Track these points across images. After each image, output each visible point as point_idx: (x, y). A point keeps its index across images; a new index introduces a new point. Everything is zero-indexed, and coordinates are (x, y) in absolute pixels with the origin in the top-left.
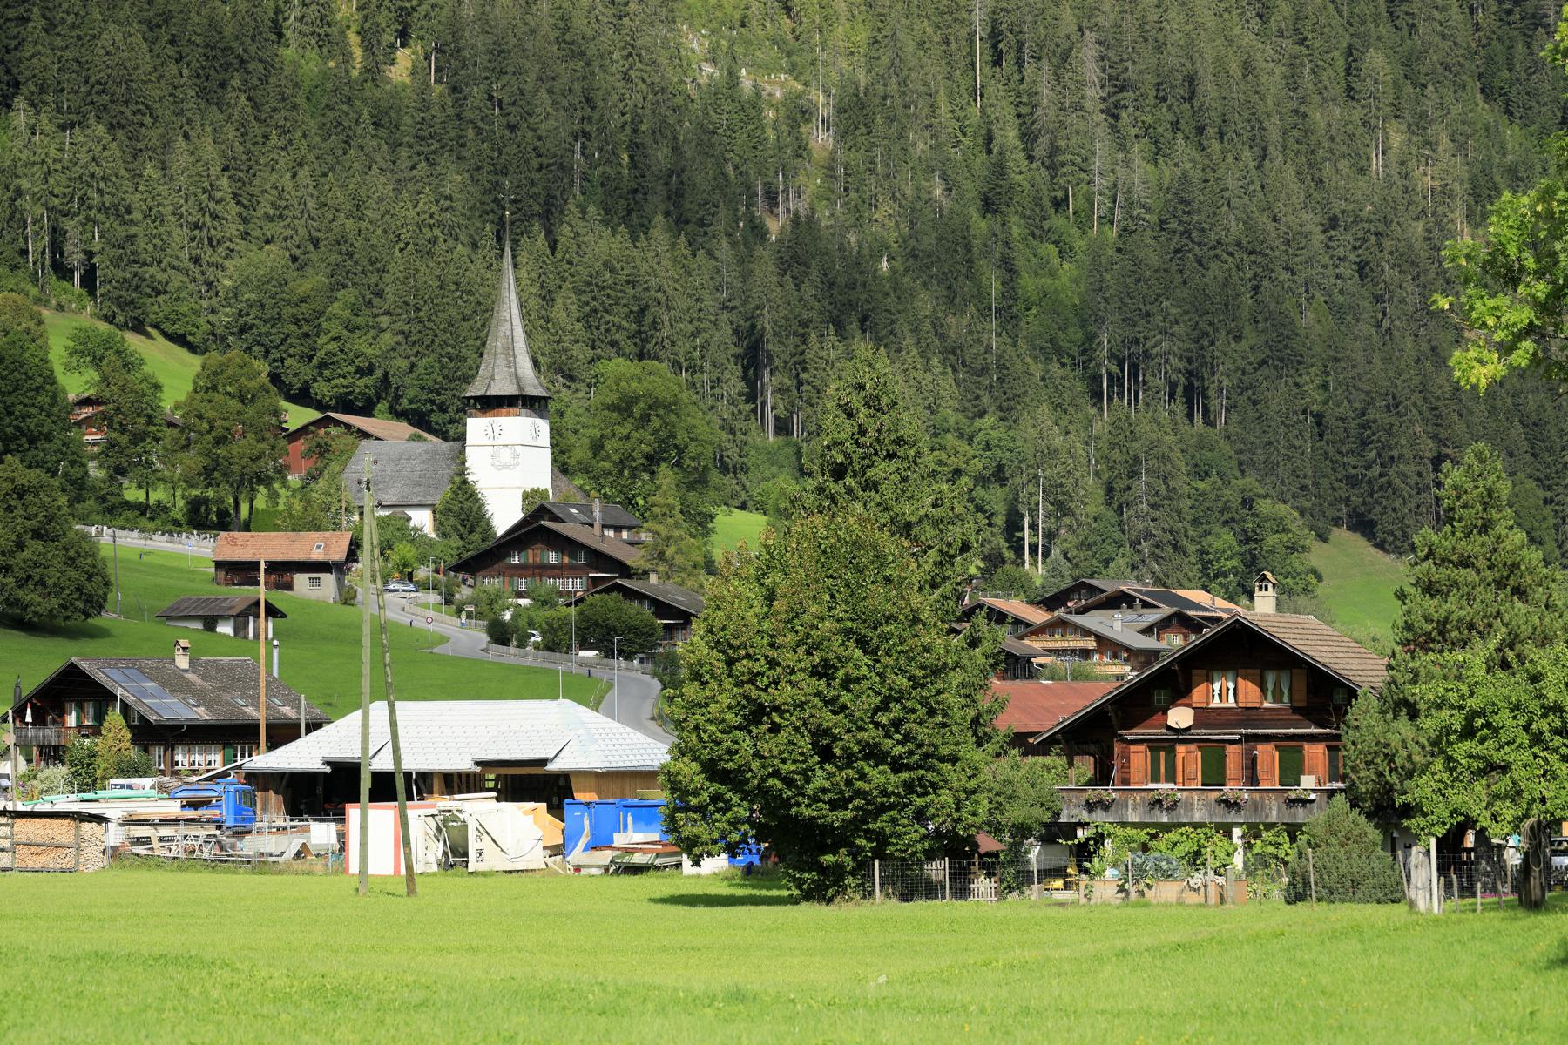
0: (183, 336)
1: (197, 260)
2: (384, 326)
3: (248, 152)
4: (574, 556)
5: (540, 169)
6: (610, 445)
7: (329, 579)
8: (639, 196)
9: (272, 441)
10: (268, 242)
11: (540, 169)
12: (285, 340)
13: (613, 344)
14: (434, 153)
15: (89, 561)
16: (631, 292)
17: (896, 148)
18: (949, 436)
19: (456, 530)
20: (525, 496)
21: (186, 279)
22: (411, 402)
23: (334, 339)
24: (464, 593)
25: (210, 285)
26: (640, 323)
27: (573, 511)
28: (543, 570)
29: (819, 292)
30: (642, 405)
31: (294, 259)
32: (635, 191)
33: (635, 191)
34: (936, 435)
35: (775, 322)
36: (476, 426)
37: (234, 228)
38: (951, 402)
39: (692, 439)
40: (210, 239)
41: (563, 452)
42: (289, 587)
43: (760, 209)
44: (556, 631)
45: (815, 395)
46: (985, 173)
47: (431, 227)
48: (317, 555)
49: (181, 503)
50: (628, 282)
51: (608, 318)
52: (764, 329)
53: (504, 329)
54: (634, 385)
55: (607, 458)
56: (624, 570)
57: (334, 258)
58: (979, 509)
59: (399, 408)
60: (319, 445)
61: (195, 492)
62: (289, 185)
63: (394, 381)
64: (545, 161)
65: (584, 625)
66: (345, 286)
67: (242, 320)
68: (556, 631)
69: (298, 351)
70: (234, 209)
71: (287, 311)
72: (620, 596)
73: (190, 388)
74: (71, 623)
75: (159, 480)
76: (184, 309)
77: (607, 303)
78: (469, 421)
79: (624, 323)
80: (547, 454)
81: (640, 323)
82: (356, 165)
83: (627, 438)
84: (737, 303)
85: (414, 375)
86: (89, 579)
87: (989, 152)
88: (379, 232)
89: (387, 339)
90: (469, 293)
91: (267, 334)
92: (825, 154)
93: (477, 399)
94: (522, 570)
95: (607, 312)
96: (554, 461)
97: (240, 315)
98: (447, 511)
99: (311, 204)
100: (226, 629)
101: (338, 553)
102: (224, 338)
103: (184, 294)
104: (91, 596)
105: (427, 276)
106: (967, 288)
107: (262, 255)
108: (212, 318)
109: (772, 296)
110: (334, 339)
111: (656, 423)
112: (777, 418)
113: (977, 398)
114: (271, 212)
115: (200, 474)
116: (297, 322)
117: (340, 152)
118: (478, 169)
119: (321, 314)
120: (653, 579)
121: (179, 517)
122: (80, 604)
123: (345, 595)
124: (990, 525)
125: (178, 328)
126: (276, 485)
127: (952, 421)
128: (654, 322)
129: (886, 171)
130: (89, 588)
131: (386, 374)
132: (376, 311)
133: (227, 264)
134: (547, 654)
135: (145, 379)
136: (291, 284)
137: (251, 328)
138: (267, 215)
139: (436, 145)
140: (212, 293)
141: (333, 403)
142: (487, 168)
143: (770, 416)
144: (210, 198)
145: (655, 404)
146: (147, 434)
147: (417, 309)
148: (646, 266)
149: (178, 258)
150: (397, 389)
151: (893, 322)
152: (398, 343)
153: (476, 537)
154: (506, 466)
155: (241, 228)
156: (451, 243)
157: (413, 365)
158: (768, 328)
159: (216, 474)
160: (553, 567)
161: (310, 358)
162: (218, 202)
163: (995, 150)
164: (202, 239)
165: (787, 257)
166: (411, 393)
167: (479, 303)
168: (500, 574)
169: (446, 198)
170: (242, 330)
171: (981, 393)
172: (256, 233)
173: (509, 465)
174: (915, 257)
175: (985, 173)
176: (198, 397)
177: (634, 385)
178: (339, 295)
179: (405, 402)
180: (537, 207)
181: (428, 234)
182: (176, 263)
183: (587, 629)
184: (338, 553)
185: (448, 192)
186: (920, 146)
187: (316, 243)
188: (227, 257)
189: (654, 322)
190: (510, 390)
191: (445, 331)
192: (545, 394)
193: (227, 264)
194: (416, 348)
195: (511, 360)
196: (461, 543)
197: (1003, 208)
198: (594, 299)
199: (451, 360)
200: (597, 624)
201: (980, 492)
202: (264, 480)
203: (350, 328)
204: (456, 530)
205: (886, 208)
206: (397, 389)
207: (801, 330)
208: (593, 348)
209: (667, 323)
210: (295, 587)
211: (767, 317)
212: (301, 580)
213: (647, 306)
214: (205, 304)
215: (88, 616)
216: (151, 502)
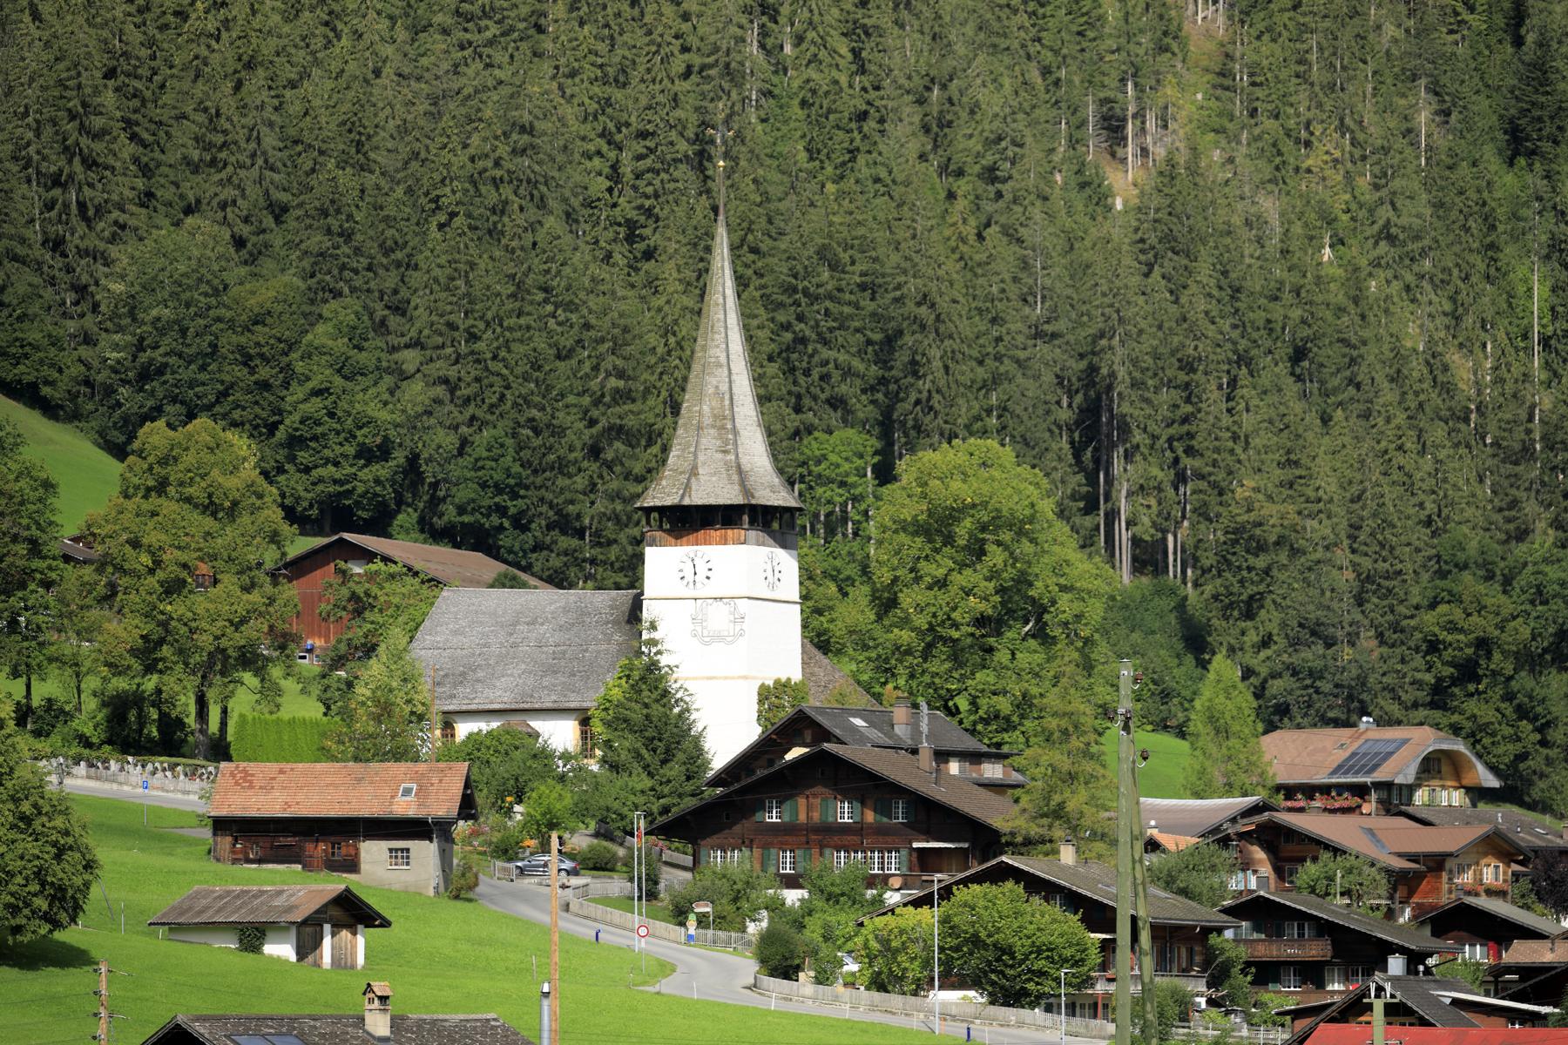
0: (34, 386)
1: (56, 245)
2: (410, 368)
3: (151, 43)
4: (884, 809)
5: (687, 75)
6: (907, 599)
7: (425, 852)
8: (870, 125)
9: (268, 589)
10: (188, 211)
11: (687, 75)
12: (224, 394)
13: (836, 403)
14: (490, 43)
15: (59, 822)
16: (869, 306)
17: (1346, 37)
18: (1466, 576)
19: (638, 756)
20: (764, 694)
21: (37, 280)
22: (461, 510)
23: (317, 393)
24: (674, 880)
25: (81, 290)
26: (885, 364)
27: (858, 722)
28: (828, 835)
29: (1214, 309)
30: (968, 523)
31: (239, 243)
32: (862, 116)
33: (862, 116)
34: (1442, 574)
35: (1135, 362)
36: (664, 564)
37: (126, 186)
38: (1469, 512)
39: (1063, 589)
40: (82, 206)
41: (819, 612)
42: (352, 866)
43: (1093, 150)
44: (896, 952)
45: (1213, 499)
46: (1512, 81)
47: (496, 183)
48: (405, 807)
49: (90, 704)
50: (863, 287)
51: (826, 353)
52: (1113, 375)
53: (715, 381)
54: (956, 485)
55: (905, 622)
56: (984, 840)
57: (317, 241)
58: (1523, 713)
59: (439, 523)
60: (354, 597)
61: (121, 684)
62: (228, 104)
63: (429, 472)
64: (697, 60)
65: (951, 942)
66: (337, 294)
67: (143, 358)
68: (896, 952)
69: (247, 414)
70: (128, 150)
71: (228, 341)
72: (1020, 889)
73: (115, 491)
74: (25, 938)
75: (51, 660)
76: (34, 336)
77: (825, 325)
78: (651, 553)
79: (858, 365)
80: (794, 615)
81: (885, 364)
82: (352, 67)
83: (942, 584)
84: (1061, 326)
85: (467, 461)
86: (58, 857)
87: (1518, 42)
88: (400, 191)
89: (416, 393)
90: (570, 307)
91: (192, 384)
92: (1211, 46)
93: (662, 510)
94: (786, 834)
95: (825, 342)
96: (805, 626)
97: (140, 347)
98: (619, 722)
99: (270, 140)
100: (281, 950)
101: (444, 803)
102: (109, 391)
103: (34, 309)
104: (61, 889)
105: (490, 272)
106: (1488, 299)
107: (181, 236)
108: (85, 352)
109: (1128, 313)
110: (317, 393)
111: (996, 556)
112: (1136, 542)
113: (1514, 504)
114: (195, 155)
115: (133, 652)
116: (247, 361)
117: (317, 43)
118: (573, 74)
119: (291, 346)
120: (1067, 855)
121: (88, 730)
122: (41, 903)
123: (457, 882)
124: (1544, 743)
125: (25, 372)
126: (276, 672)
127: (1473, 546)
128: (914, 362)
129: (1327, 77)
130: (58, 873)
131: (413, 459)
132: (394, 340)
133: (114, 251)
134: (876, 996)
135: (25, 472)
136: (234, 291)
137: (161, 371)
138: (187, 161)
139: (494, 30)
140: (84, 306)
141: (314, 512)
142: (590, 72)
143: (1123, 536)
144: (82, 128)
145: (996, 522)
146: (28, 573)
147: (473, 337)
148: (895, 258)
149: (23, 241)
150: (435, 486)
151: (1353, 361)
152: (437, 401)
153: (674, 770)
154: (719, 638)
155: (140, 183)
156: (532, 213)
157: (464, 442)
158: (1122, 373)
159: (166, 651)
160: (845, 829)
161: (272, 428)
162: (97, 136)
163: (1530, 38)
164: (66, 206)
165: (1153, 239)
166: (463, 494)
167: (587, 326)
168: (745, 843)
169: (523, 130)
170: (145, 375)
171: (1522, 495)
172: (166, 193)
173: (728, 634)
174: (1392, 239)
175: (1512, 81)
176: (130, 505)
177: (956, 485)
178: (326, 310)
179: (449, 513)
180: (683, 147)
181: (491, 197)
182: (20, 250)
183: (957, 949)
184: (444, 803)
185: (527, 118)
186: (1390, 30)
187: (279, 212)
188: (113, 239)
189: (914, 362)
190: (728, 495)
191: (526, 378)
192: (793, 503)
193: (114, 251)
194: (471, 410)
195: (726, 433)
196: (648, 783)
197: (1546, 146)
198: (800, 318)
199: (537, 432)
200: (976, 941)
201: (1524, 681)
202: (249, 659)
203: (347, 371)
204: (638, 756)
205: (1329, 145)
206: (435, 486)
207: (1182, 377)
208: (798, 410)
209: (937, 364)
210: (363, 867)
211: (1120, 351)
212: (373, 852)
213: (900, 333)
214: (72, 326)
215: (57, 925)
216: (36, 702)
